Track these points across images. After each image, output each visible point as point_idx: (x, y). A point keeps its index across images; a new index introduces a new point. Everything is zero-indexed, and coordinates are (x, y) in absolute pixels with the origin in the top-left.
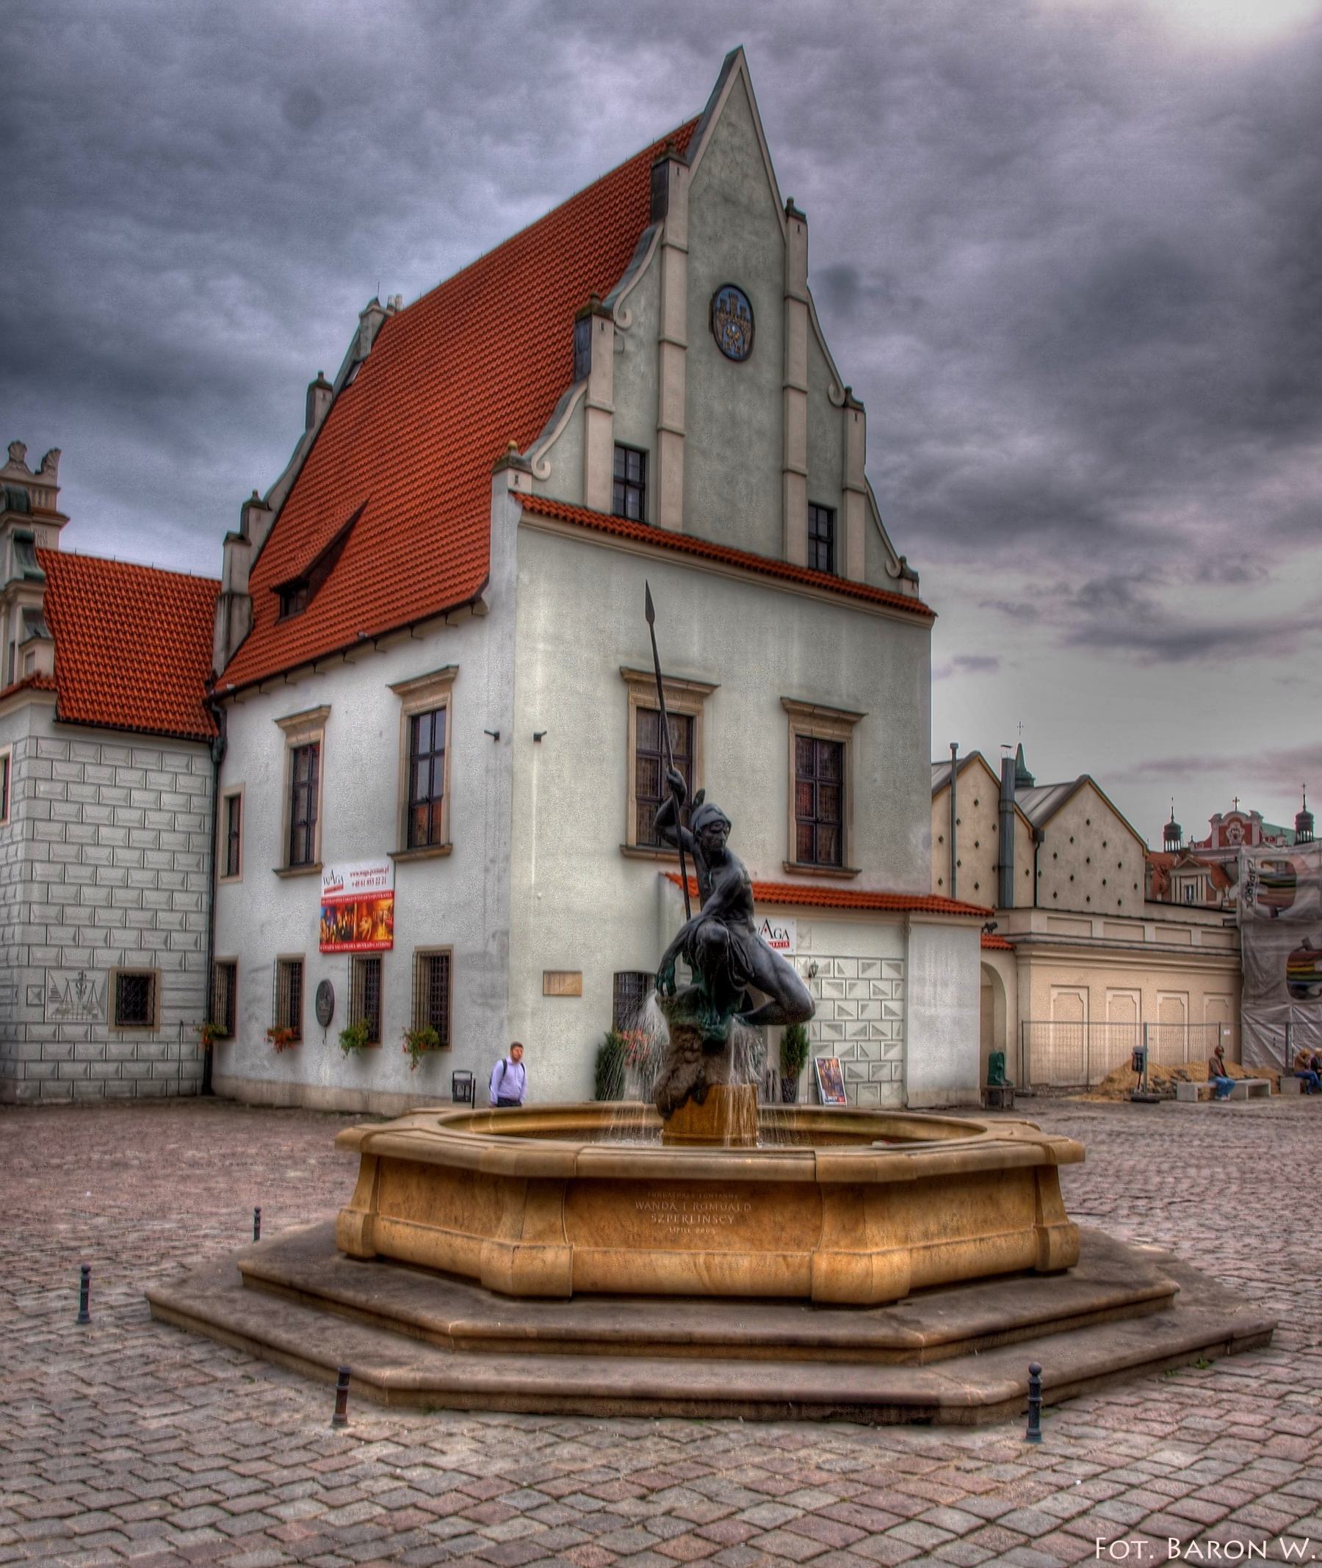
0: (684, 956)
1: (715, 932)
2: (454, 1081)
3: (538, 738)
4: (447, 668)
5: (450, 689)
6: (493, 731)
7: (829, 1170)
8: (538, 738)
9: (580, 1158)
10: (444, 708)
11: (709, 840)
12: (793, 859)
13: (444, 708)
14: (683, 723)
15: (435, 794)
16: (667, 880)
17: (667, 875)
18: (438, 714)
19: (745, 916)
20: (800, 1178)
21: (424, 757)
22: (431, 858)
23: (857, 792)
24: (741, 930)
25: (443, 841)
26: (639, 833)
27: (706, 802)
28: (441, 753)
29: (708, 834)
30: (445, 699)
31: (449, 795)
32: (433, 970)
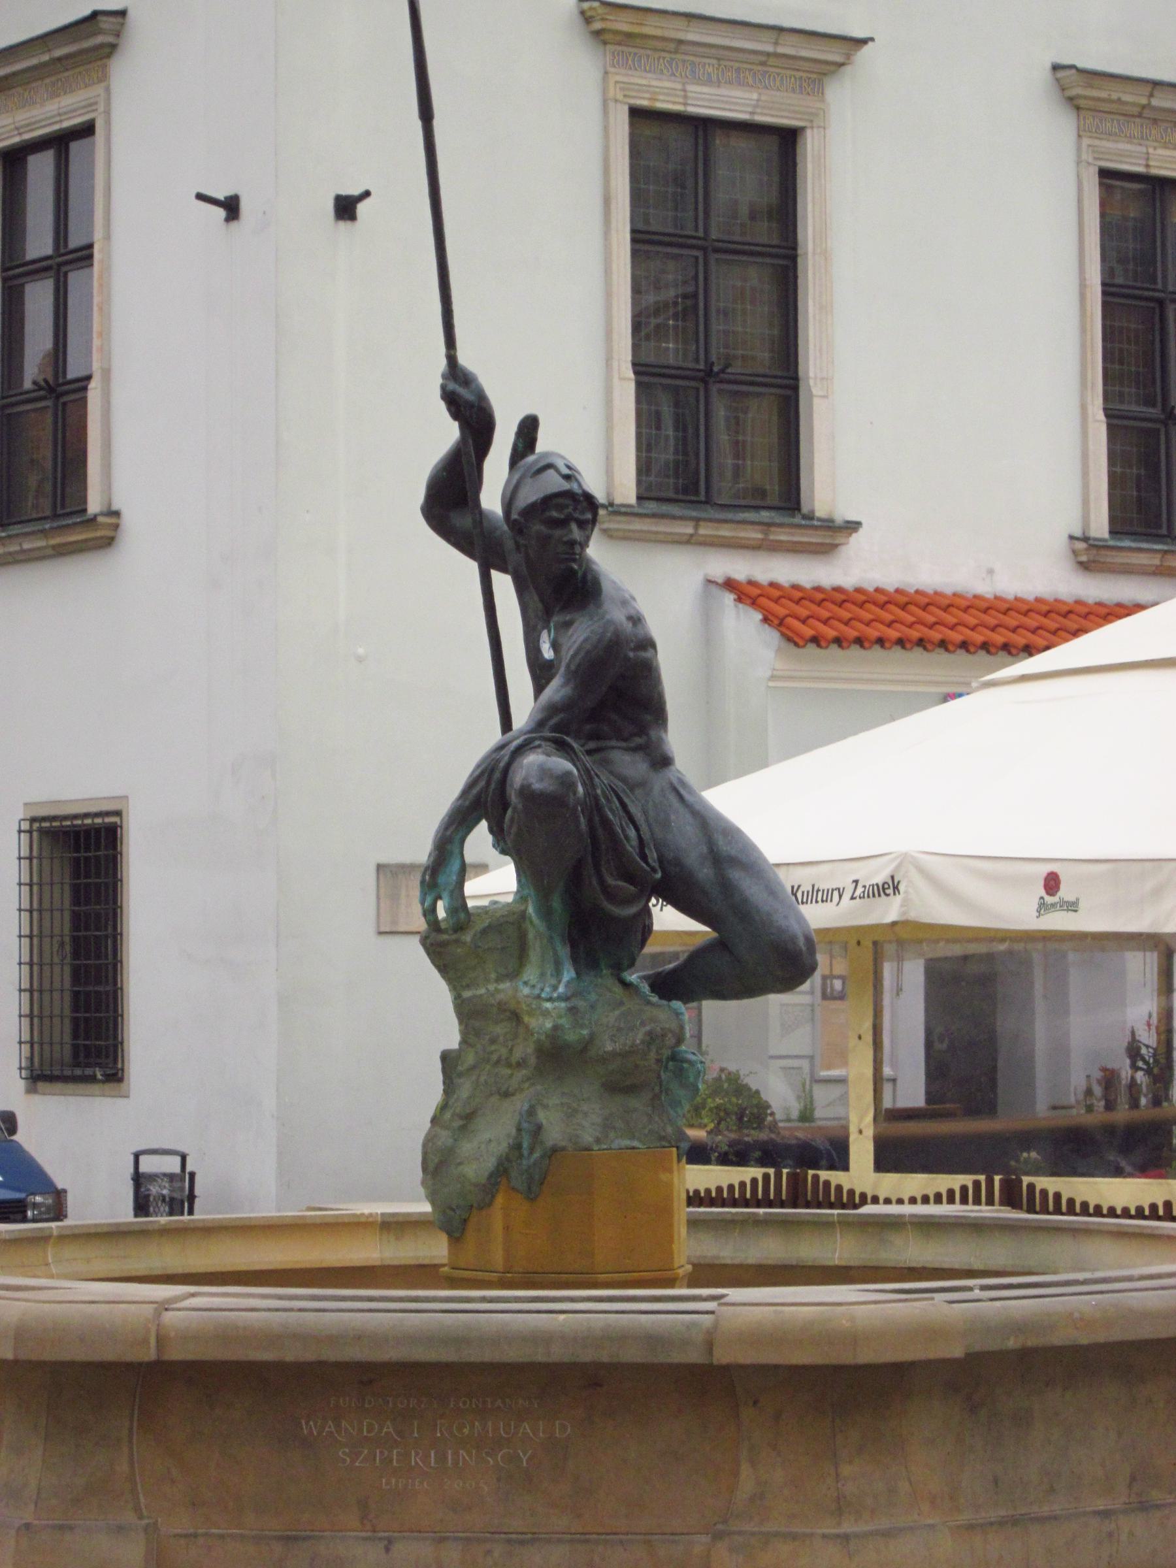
0: (497, 831)
1: (544, 772)
2: (139, 1179)
3: (346, 208)
4: (95, 15)
5: (104, 77)
6: (362, 208)
7: (756, 1337)
8: (346, 208)
9: (169, 1317)
10: (87, 130)
11: (544, 540)
12: (1100, 527)
13: (87, 130)
14: (771, 144)
15: (73, 371)
16: (729, 598)
17: (730, 585)
18: (75, 147)
19: (642, 730)
20: (677, 1357)
21: (40, 268)
22: (62, 552)
23: (131, 860)
24: (631, 765)
25: (94, 505)
26: (644, 468)
27: (540, 447)
28: (84, 256)
29: (537, 527)
30: (91, 105)
31: (107, 373)
32: (79, 868)
